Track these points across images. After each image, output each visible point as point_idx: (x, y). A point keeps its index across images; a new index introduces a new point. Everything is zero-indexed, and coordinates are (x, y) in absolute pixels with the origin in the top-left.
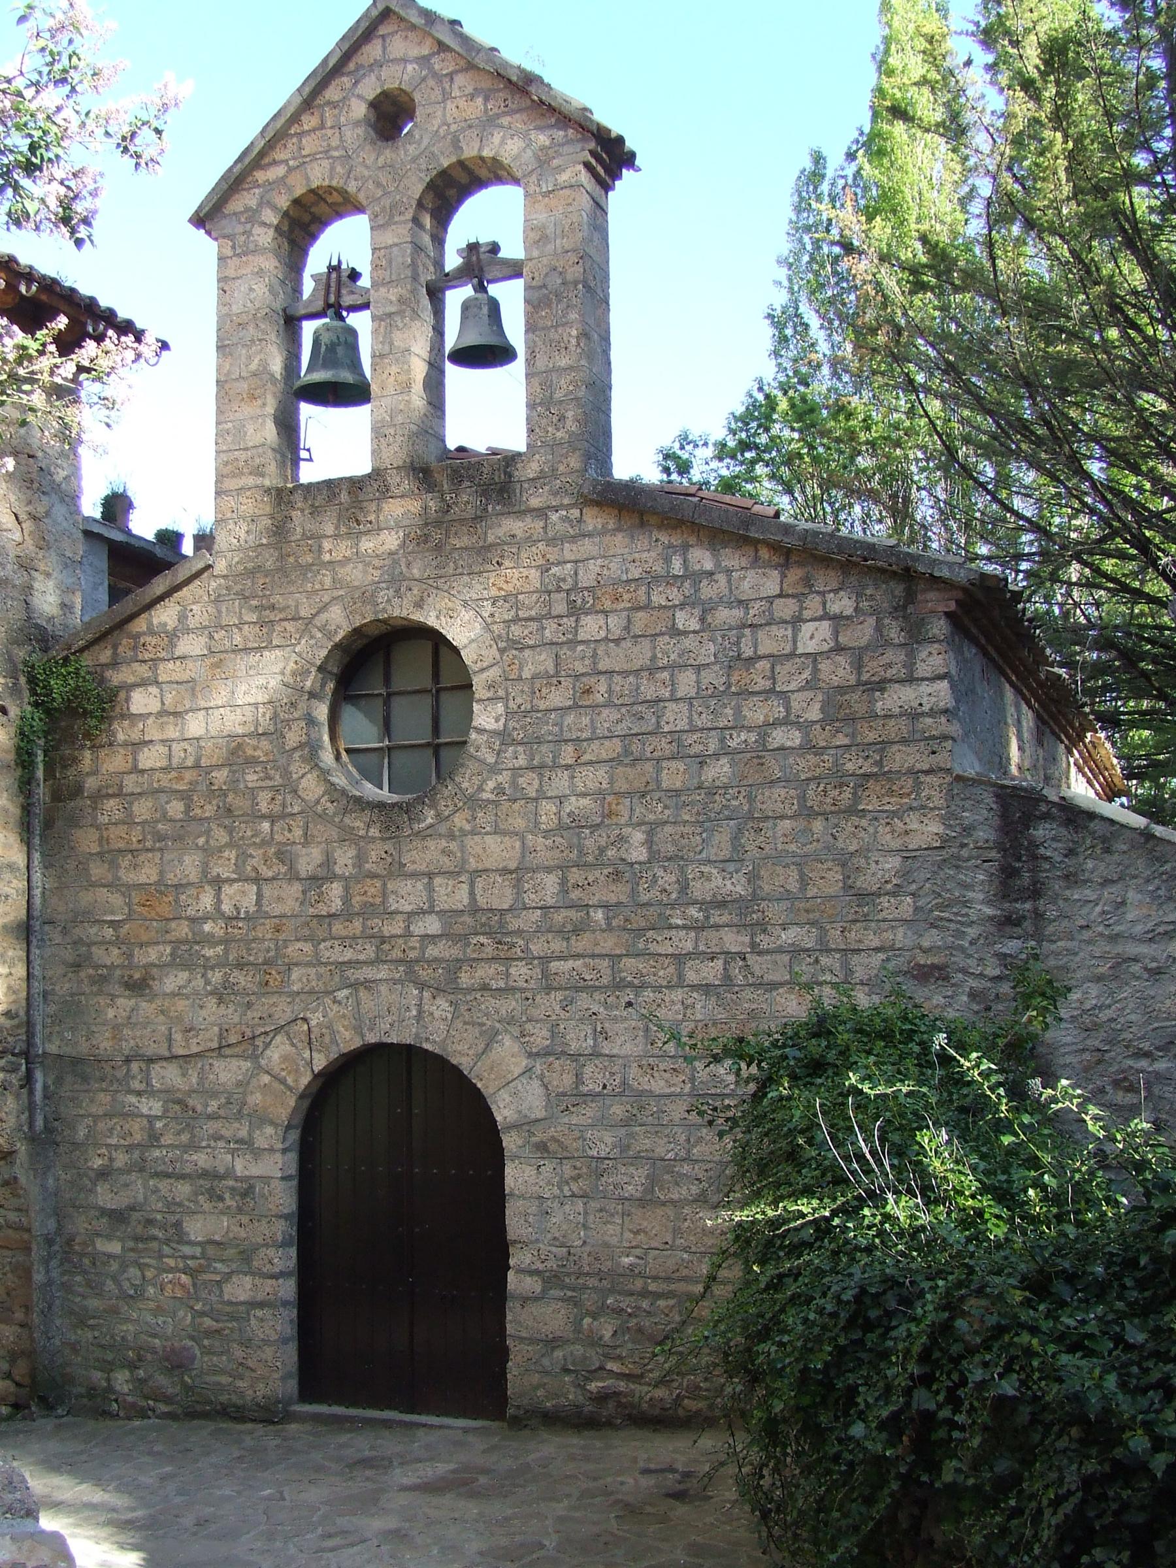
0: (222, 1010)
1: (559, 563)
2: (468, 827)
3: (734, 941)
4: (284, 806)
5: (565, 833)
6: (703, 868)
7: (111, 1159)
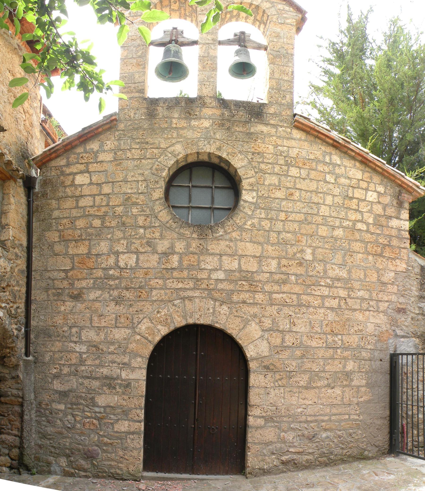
0: (117, 307)
1: (281, 146)
2: (238, 238)
3: (343, 293)
4: (151, 222)
5: (280, 246)
6: (332, 266)
7: (61, 370)
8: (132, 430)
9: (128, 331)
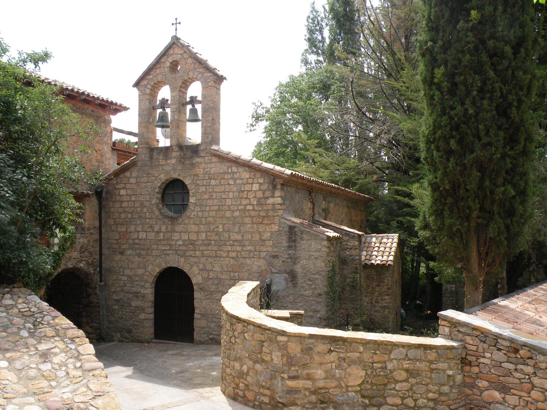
3: (239, 249)
8: (146, 318)
9: (144, 270)
